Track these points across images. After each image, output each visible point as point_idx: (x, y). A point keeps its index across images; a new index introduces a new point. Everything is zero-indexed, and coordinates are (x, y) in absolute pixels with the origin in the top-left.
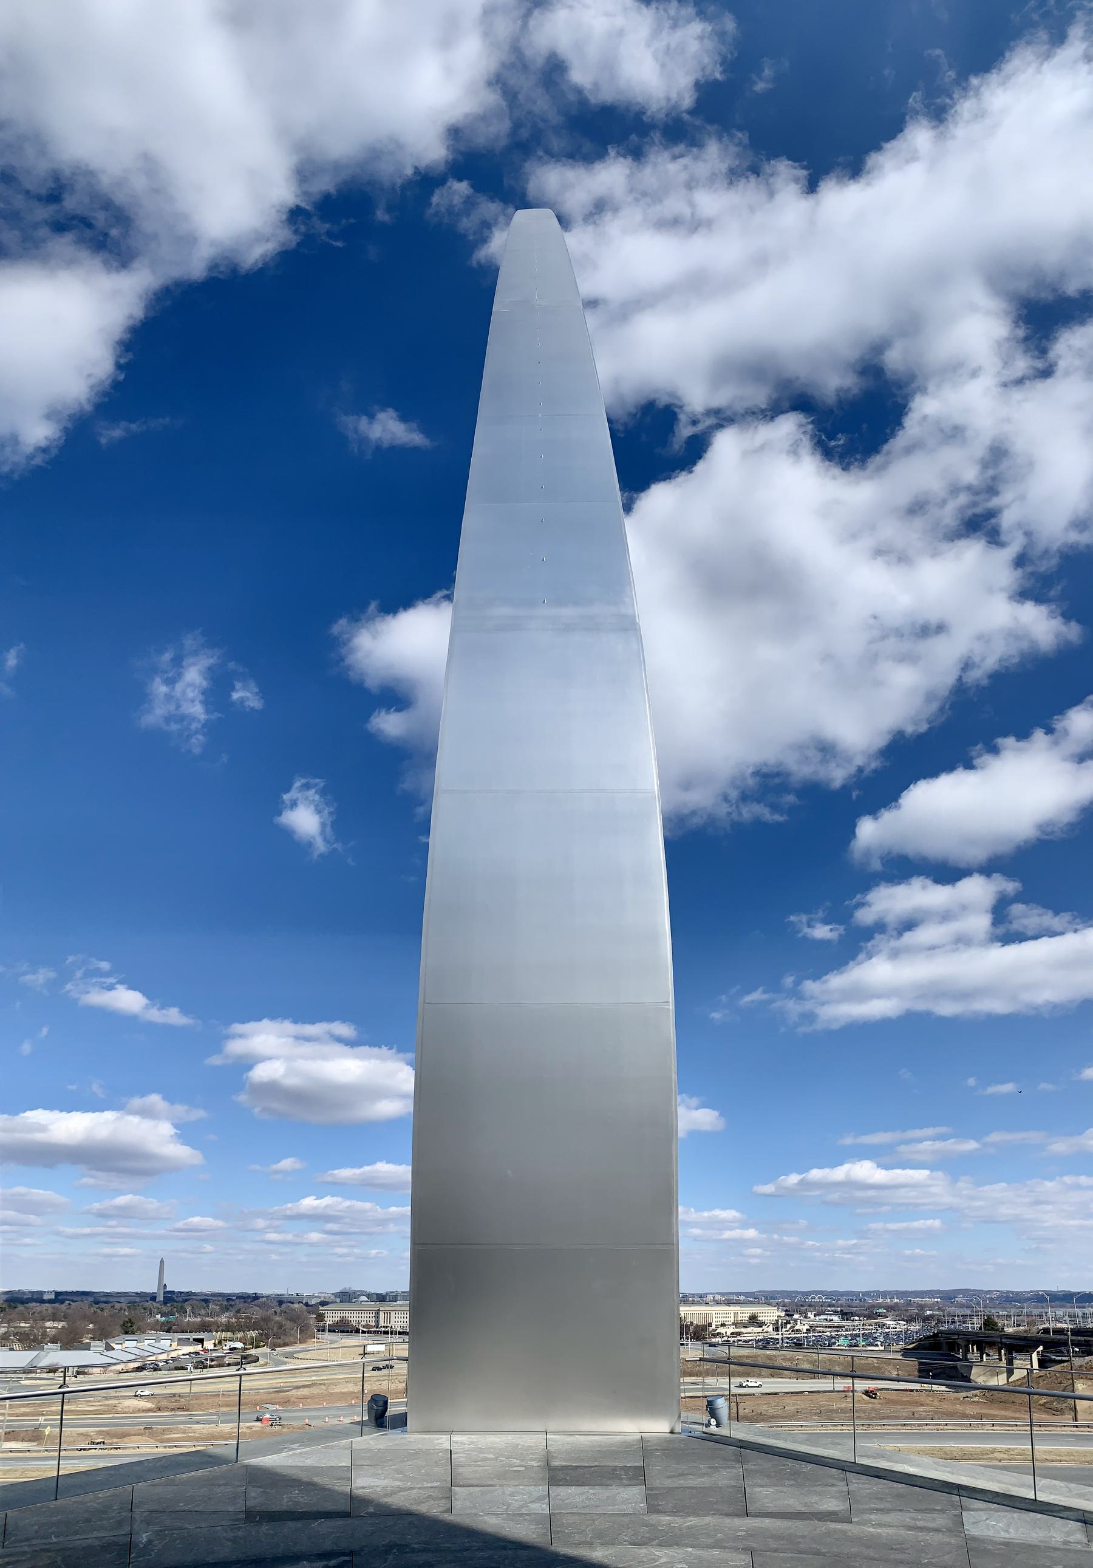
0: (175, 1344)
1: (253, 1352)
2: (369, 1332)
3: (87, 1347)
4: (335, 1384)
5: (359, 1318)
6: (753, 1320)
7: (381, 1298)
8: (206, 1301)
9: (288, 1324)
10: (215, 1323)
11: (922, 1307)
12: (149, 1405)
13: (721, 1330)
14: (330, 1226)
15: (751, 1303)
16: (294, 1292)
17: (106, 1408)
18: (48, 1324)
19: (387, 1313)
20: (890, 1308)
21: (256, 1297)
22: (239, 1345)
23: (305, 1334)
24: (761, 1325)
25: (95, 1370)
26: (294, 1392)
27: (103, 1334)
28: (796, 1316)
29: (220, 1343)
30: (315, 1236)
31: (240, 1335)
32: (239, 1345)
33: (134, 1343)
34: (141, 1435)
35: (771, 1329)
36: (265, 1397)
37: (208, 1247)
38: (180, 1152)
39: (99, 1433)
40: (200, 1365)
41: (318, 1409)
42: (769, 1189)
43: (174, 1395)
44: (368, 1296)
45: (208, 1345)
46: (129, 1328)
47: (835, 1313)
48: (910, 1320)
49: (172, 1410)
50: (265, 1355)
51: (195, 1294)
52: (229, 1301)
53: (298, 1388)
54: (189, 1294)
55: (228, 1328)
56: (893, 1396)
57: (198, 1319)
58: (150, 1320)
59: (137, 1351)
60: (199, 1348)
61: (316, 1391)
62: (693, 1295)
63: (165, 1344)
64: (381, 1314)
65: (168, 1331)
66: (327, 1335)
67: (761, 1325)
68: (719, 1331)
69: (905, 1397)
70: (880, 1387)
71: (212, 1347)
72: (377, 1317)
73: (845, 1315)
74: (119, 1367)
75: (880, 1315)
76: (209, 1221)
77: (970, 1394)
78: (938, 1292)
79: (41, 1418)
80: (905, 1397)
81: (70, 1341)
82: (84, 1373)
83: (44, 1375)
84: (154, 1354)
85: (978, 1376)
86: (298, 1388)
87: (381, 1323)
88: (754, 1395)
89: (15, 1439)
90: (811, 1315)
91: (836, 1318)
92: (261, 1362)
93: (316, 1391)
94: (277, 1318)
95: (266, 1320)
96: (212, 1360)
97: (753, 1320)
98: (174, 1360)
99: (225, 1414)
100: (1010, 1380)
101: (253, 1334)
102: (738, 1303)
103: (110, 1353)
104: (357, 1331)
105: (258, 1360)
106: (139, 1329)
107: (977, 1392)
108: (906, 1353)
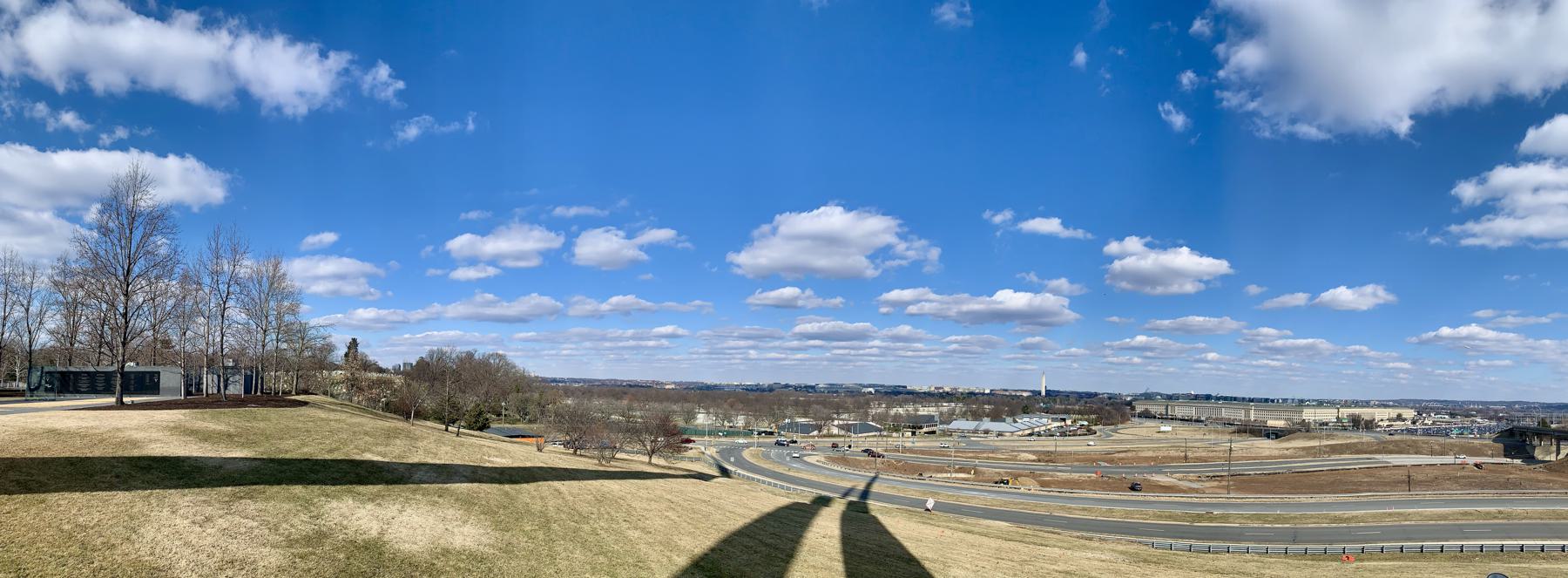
0: (1050, 421)
1: (1094, 428)
2: (1162, 418)
3: (1004, 421)
4: (1142, 451)
5: (1155, 409)
6: (1399, 418)
7: (1170, 397)
8: (1068, 396)
9: (1114, 412)
10: (1073, 409)
11: (1496, 411)
12: (1034, 457)
13: (1380, 423)
14: (1149, 354)
15: (1396, 406)
16: (1117, 392)
17: (1010, 457)
18: (986, 406)
19: (1173, 406)
20: (1479, 411)
21: (1096, 394)
22: (1086, 423)
23: (1124, 419)
24: (1404, 420)
25: (1007, 434)
26: (1116, 455)
27: (1012, 414)
28: (1424, 415)
29: (1075, 421)
30: (1136, 360)
31: (1086, 417)
32: (1086, 423)
33: (1028, 419)
34: (1028, 476)
35: (1410, 423)
36: (1099, 457)
37: (1075, 365)
38: (1071, 315)
39: (1006, 473)
40: (1063, 434)
41: (1129, 467)
42: (1414, 339)
43: (1048, 452)
44: (1161, 395)
45: (1069, 422)
46: (1026, 410)
47: (1447, 414)
48: (1491, 419)
49: (1047, 461)
50: (1100, 430)
51: (1062, 392)
52: (1080, 396)
53: (1119, 452)
54: (1058, 392)
55: (1080, 413)
56: (1492, 467)
57: (1063, 407)
58: (1037, 406)
59: (1029, 424)
60: (1063, 424)
61: (1130, 455)
62: (1362, 401)
63: (1044, 420)
64: (1169, 407)
65: (1047, 413)
66: (1136, 420)
67: (1404, 420)
68: (1380, 423)
69: (1500, 468)
70: (1483, 461)
71: (1070, 424)
72: (1167, 409)
73: (1452, 415)
74: (1020, 433)
75: (1473, 416)
76: (1081, 351)
77: (1537, 466)
78: (1505, 402)
79: (977, 461)
80: (1500, 468)
81: (996, 417)
82: (1002, 435)
83: (982, 435)
84: (1021, 430)
85: (1539, 454)
86: (1119, 452)
87: (1169, 413)
88: (1273, 401)
89: (964, 472)
90: (1432, 415)
91: (1447, 417)
92: (1098, 434)
93: (1130, 455)
94: (1108, 408)
95: (1101, 409)
96: (1070, 431)
97: (1399, 418)
98: (1049, 430)
99: (1075, 467)
100: (1559, 458)
101: (1094, 416)
102: (1389, 406)
103: (1016, 425)
104: (1155, 417)
105: (1095, 433)
106: (1031, 411)
107: (1541, 465)
108: (1495, 440)
